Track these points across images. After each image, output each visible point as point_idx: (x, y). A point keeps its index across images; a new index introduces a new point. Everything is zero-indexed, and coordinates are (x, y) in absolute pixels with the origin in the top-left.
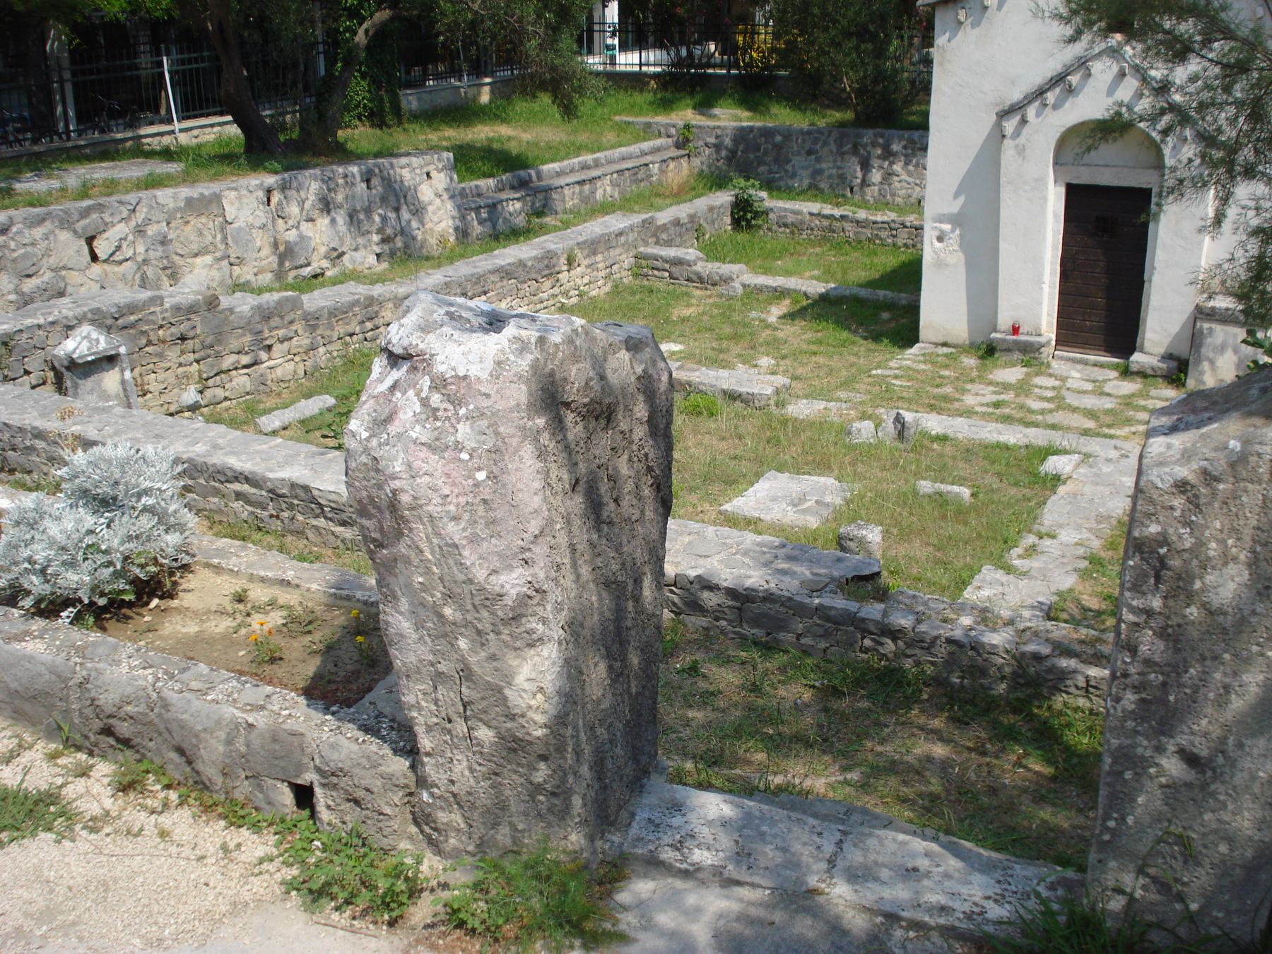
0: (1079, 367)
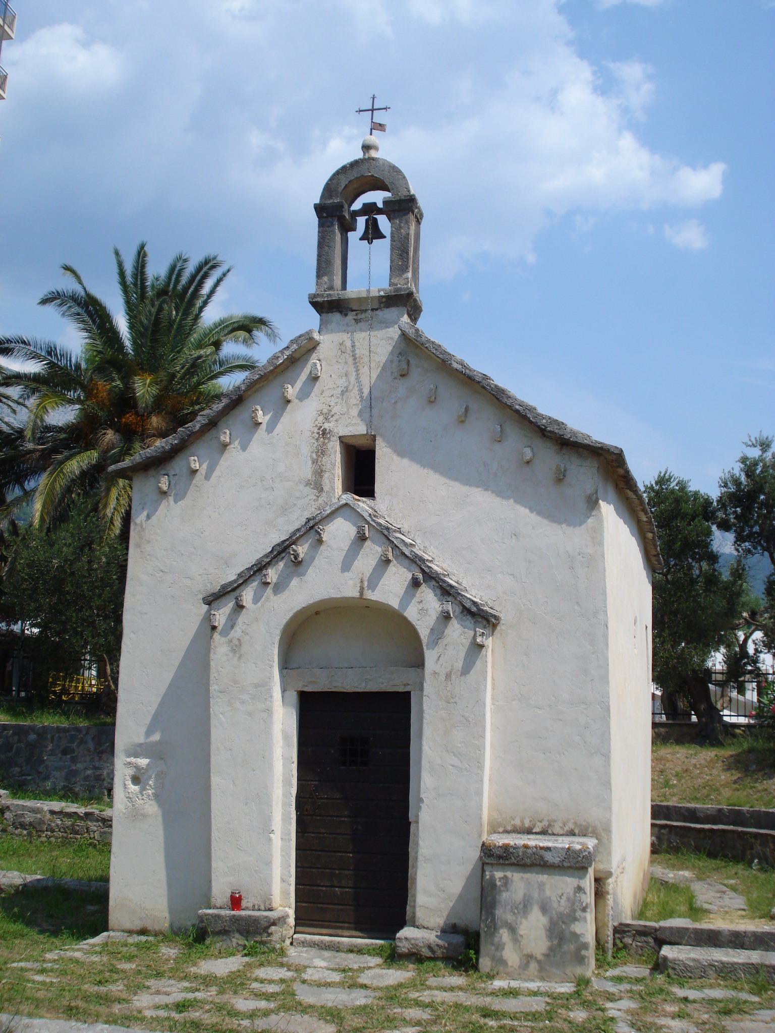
0: (327, 954)
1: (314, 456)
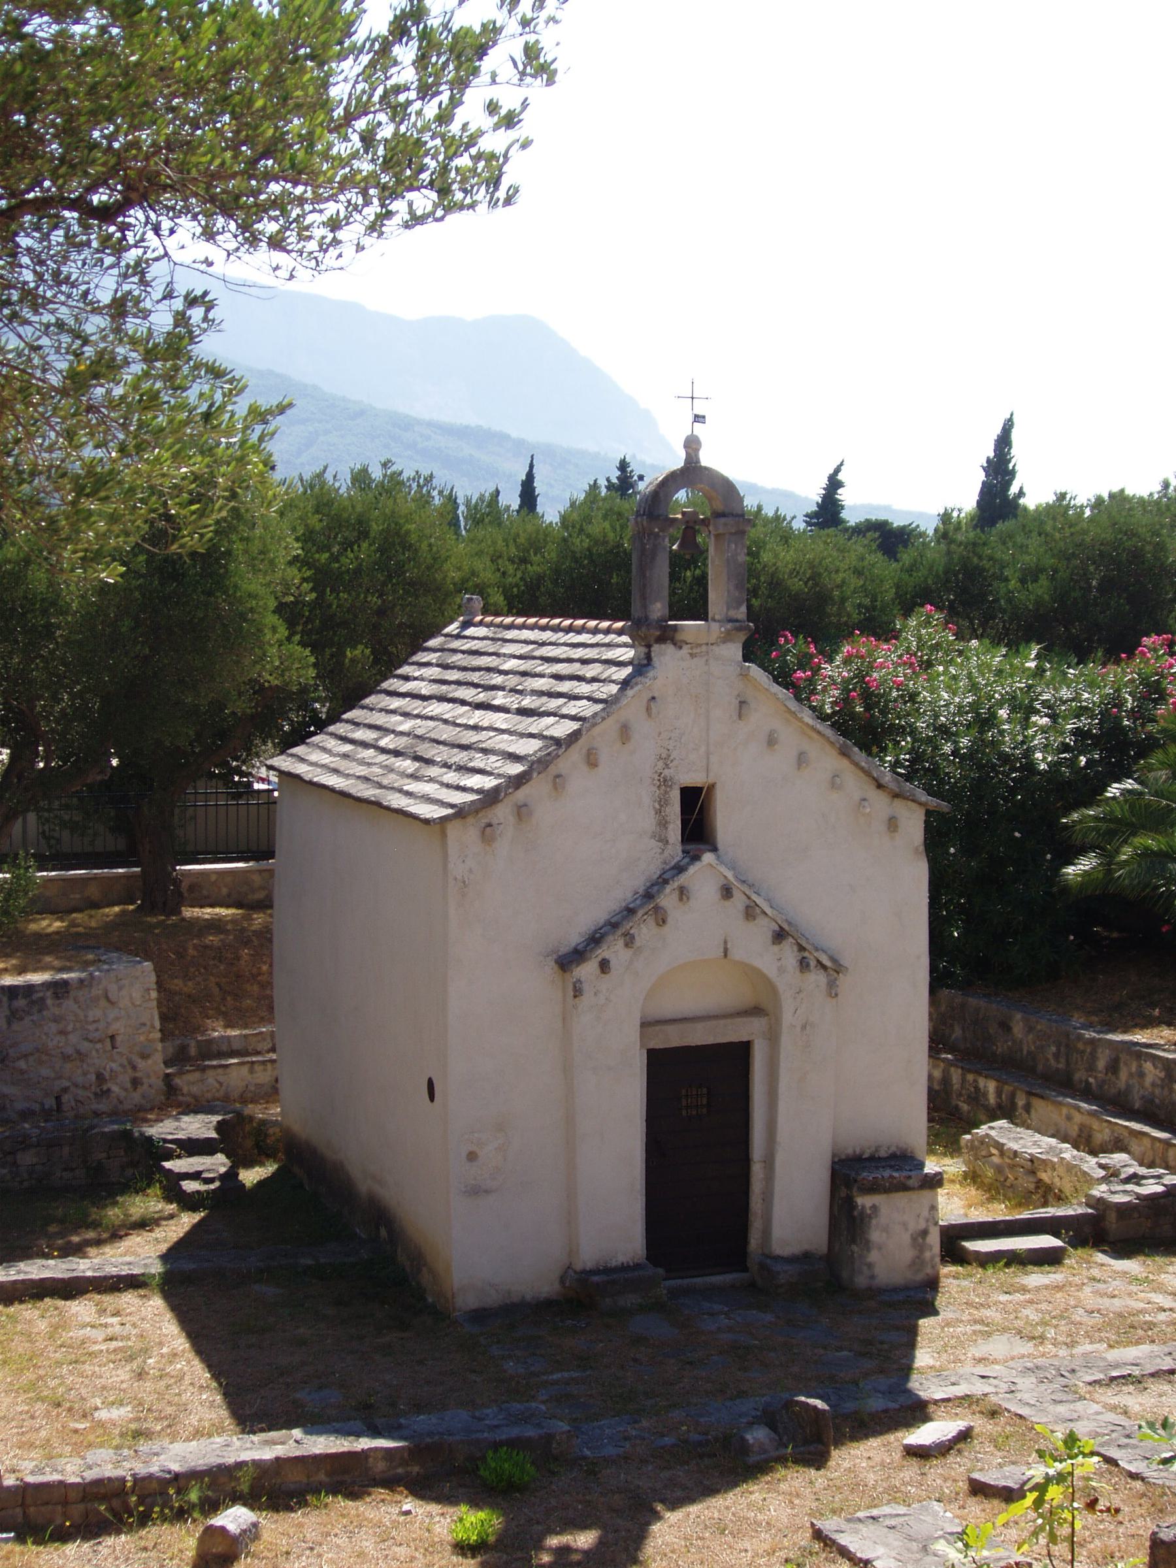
1: (657, 806)
